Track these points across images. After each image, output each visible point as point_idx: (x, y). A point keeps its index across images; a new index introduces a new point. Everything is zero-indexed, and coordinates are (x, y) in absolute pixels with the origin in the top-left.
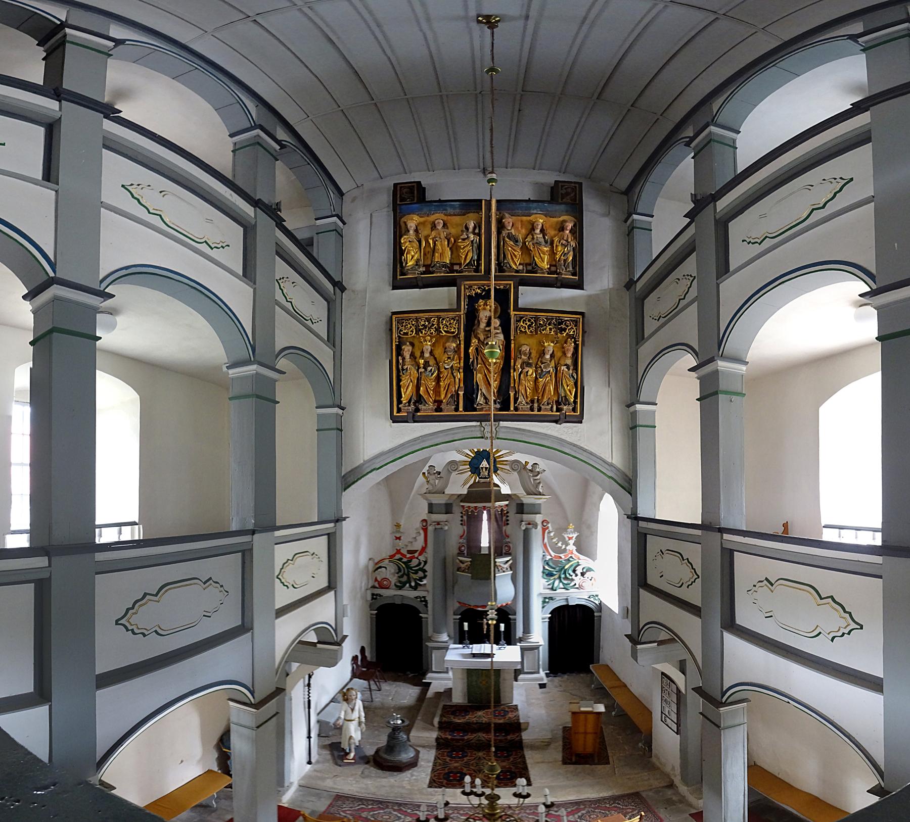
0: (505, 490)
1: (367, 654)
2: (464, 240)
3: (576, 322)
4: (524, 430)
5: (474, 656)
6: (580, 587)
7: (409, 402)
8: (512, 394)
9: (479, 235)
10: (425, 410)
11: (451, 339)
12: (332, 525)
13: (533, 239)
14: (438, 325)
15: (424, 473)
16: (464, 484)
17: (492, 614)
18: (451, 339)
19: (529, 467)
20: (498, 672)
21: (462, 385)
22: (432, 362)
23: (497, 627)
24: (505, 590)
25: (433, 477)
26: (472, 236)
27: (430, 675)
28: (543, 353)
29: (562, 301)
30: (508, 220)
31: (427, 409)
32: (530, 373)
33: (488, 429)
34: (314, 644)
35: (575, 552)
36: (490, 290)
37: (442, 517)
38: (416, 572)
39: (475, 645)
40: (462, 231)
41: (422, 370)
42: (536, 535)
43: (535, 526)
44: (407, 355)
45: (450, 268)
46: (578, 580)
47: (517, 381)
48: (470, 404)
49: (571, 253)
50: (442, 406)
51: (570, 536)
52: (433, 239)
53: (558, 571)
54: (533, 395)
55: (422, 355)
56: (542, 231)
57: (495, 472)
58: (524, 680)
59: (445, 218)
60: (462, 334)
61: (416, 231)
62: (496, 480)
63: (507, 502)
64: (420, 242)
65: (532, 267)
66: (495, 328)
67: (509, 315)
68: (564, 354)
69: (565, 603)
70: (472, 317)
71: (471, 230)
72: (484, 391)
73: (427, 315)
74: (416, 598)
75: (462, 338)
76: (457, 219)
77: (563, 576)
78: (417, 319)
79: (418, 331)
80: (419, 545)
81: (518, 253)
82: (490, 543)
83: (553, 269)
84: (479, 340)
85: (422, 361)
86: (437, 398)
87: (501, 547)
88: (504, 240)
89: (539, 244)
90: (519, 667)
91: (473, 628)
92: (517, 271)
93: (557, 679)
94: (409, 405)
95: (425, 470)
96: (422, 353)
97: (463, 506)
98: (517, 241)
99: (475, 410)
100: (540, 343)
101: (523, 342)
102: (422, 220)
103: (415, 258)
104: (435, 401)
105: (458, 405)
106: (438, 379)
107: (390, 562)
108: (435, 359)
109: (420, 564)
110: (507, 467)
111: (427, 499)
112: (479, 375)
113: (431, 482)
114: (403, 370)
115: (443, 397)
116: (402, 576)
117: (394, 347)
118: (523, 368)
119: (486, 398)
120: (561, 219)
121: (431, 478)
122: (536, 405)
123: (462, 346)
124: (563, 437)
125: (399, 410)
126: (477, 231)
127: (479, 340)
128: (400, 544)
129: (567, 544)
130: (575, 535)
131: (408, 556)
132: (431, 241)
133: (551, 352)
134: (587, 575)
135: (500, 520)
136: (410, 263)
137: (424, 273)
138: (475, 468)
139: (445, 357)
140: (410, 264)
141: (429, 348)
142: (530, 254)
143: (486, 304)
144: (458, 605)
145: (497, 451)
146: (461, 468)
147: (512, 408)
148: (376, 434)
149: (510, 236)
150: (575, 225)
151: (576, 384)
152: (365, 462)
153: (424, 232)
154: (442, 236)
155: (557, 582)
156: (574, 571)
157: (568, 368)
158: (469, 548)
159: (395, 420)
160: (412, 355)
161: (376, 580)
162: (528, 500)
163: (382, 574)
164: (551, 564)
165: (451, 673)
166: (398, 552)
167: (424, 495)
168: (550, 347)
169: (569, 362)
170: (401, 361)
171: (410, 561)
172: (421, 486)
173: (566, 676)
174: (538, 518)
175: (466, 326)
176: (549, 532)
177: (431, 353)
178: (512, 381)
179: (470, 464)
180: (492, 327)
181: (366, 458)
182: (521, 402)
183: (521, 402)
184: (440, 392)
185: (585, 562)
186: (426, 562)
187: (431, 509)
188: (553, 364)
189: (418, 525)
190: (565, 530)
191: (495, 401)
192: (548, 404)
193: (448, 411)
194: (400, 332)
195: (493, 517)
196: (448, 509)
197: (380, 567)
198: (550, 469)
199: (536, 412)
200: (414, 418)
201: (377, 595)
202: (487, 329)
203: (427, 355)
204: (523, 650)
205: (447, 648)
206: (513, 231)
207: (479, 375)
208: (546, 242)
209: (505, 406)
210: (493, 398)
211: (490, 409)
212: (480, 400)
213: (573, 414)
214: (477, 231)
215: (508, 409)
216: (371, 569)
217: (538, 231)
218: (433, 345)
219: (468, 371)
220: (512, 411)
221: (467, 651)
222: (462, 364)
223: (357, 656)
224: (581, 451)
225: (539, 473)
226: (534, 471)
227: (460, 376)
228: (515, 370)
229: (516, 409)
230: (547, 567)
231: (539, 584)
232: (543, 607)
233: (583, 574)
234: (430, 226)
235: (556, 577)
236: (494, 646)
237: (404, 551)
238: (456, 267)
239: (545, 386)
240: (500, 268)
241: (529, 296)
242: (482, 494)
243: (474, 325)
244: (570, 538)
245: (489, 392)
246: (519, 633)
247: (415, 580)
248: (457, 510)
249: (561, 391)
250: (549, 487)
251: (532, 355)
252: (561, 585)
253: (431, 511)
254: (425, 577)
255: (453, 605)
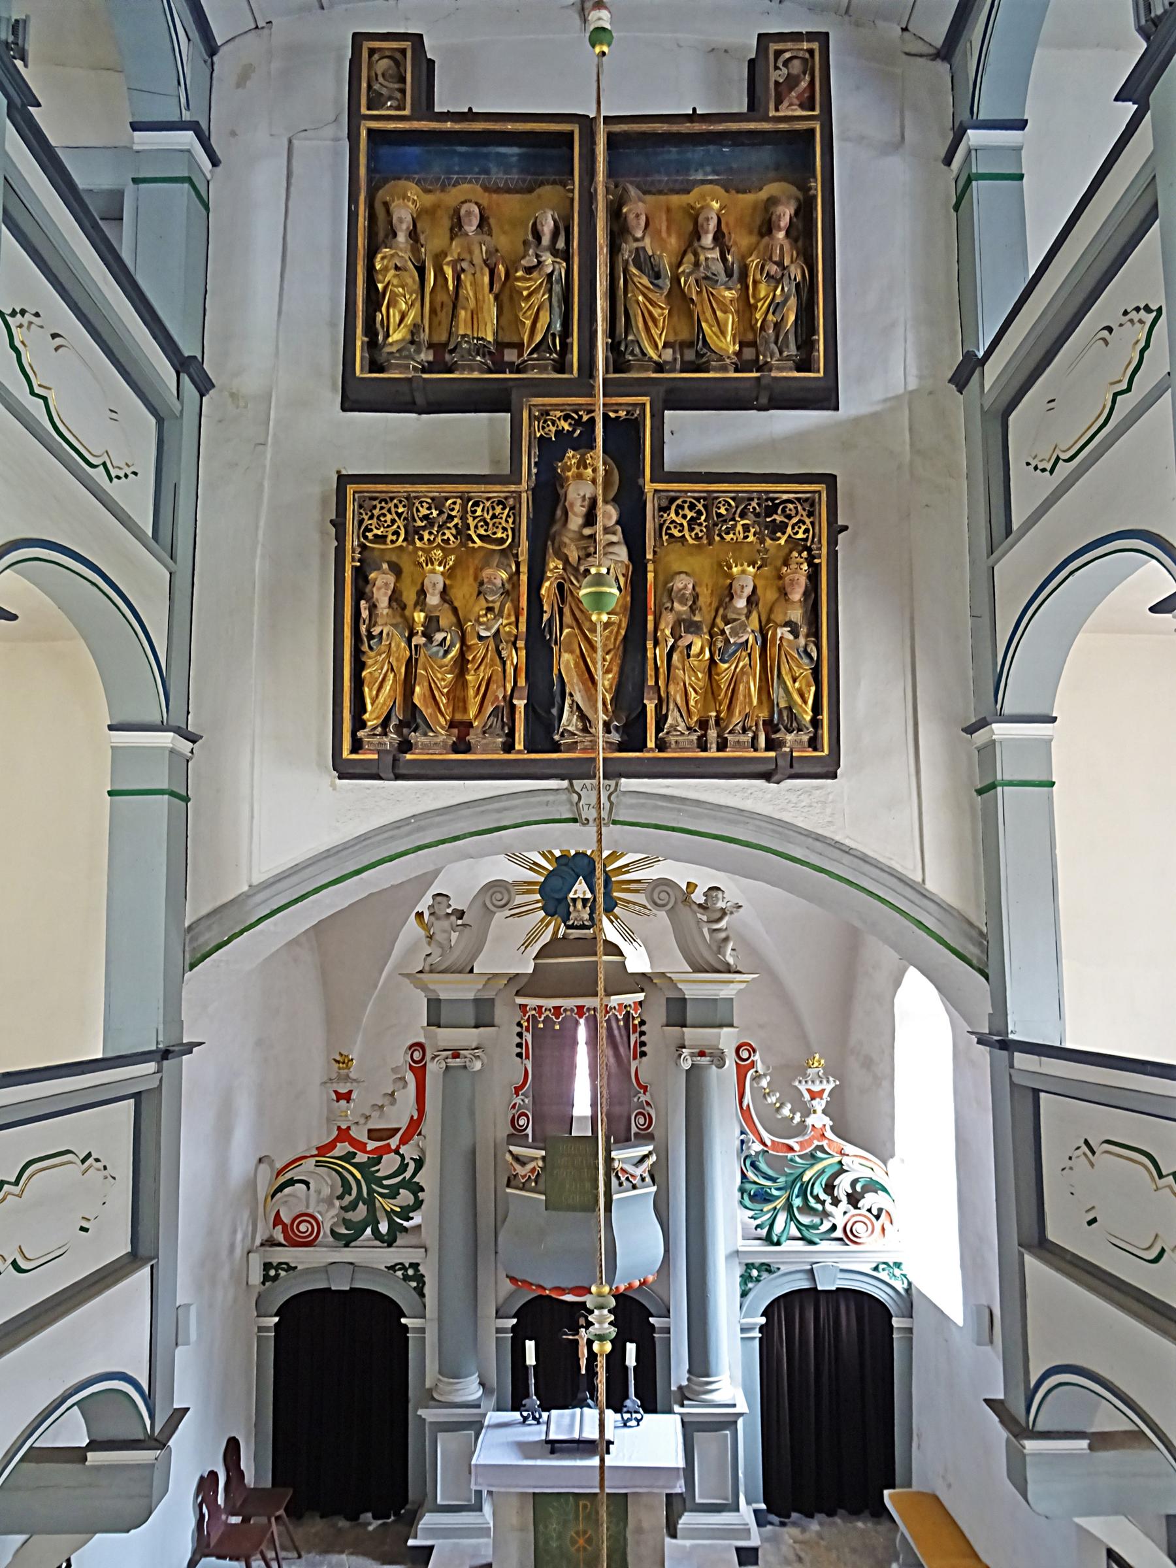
0: (637, 961)
1: (246, 1464)
2: (529, 270)
3: (811, 505)
4: (683, 800)
5: (554, 1447)
6: (849, 1237)
7: (385, 724)
8: (650, 707)
9: (566, 256)
10: (426, 747)
11: (496, 560)
12: (151, 1067)
13: (697, 264)
14: (463, 518)
15: (420, 915)
16: (527, 944)
17: (602, 1323)
18: (496, 560)
19: (698, 897)
20: (620, 1502)
21: (522, 682)
22: (446, 620)
23: (617, 1355)
24: (639, 1242)
25: (445, 924)
26: (548, 259)
27: (429, 1520)
28: (730, 594)
29: (773, 446)
30: (636, 209)
31: (432, 744)
32: (695, 649)
33: (589, 798)
34: (77, 1455)
35: (829, 1134)
36: (592, 421)
37: (468, 1036)
38: (393, 1193)
39: (554, 1413)
40: (525, 243)
41: (419, 640)
42: (721, 1083)
43: (719, 1059)
44: (382, 599)
45: (494, 355)
46: (840, 1215)
47: (663, 670)
48: (543, 734)
49: (793, 301)
50: (472, 738)
51: (816, 1088)
52: (454, 264)
53: (790, 1191)
54: (706, 708)
55: (421, 602)
56: (719, 237)
57: (609, 910)
58: (695, 1533)
59: (485, 199)
60: (524, 545)
61: (413, 235)
62: (611, 933)
63: (640, 996)
64: (421, 271)
65: (696, 354)
66: (607, 530)
67: (642, 492)
68: (784, 593)
69: (806, 1285)
70: (549, 496)
71: (546, 240)
72: (578, 698)
73: (435, 490)
74: (392, 1268)
75: (523, 557)
76: (511, 204)
77: (797, 1202)
78: (409, 500)
79: (413, 533)
80: (400, 1115)
81: (660, 313)
82: (594, 1105)
83: (749, 353)
84: (566, 561)
85: (419, 617)
86: (459, 717)
87: (624, 1121)
88: (626, 271)
89: (711, 279)
90: (679, 1487)
91: (550, 1361)
92: (660, 368)
93: (789, 1534)
94: (385, 734)
95: (423, 906)
96: (422, 592)
97: (523, 1007)
98: (658, 276)
99: (556, 748)
100: (723, 569)
101: (676, 567)
102: (429, 199)
103: (409, 320)
104: (452, 724)
105: (511, 734)
106: (462, 663)
107: (318, 1164)
108: (455, 610)
109: (403, 1167)
110: (641, 898)
111: (424, 988)
112: (566, 656)
113: (439, 937)
114: (370, 636)
115: (472, 712)
116: (353, 1206)
117: (348, 574)
118: (677, 637)
119: (583, 717)
120: (763, 195)
121: (439, 927)
122: (712, 734)
123: (524, 578)
124: (787, 817)
125: (357, 746)
126: (561, 244)
127: (566, 561)
128: (349, 1113)
129: (808, 1112)
130: (828, 1087)
131: (372, 1145)
132: (449, 272)
133: (748, 591)
134: (870, 1200)
135: (623, 1041)
136: (397, 336)
137: (428, 368)
138: (554, 900)
139: (479, 608)
140: (395, 337)
141: (440, 581)
142: (690, 314)
143: (582, 464)
144: (508, 1286)
145: (614, 856)
146: (519, 899)
147: (651, 744)
148: (291, 809)
149: (644, 262)
150: (797, 213)
151: (816, 673)
152: (255, 889)
153: (435, 240)
154: (478, 260)
155: (782, 1218)
156: (829, 1188)
157: (795, 633)
158: (538, 1119)
159: (345, 771)
160: (395, 598)
161: (278, 1220)
162: (696, 988)
163: (292, 1203)
164: (763, 1166)
165: (487, 1508)
166: (344, 1135)
167: (416, 978)
168: (746, 576)
169: (796, 614)
170: (365, 614)
171: (378, 1161)
172: (412, 950)
173: (814, 1526)
174: (727, 1039)
175: (533, 524)
176: (757, 1077)
177: (444, 593)
178: (650, 672)
179: (543, 889)
180: (599, 527)
181: (257, 879)
182: (674, 728)
183: (674, 728)
184: (465, 701)
185: (859, 1164)
186: (419, 1163)
187: (436, 1015)
188: (754, 623)
189: (401, 1058)
190: (802, 1071)
191: (607, 725)
192: (744, 730)
193: (487, 750)
194: (366, 525)
195: (602, 1032)
196: (482, 1014)
197: (291, 1182)
198: (752, 902)
199: (713, 753)
200: (397, 768)
201: (279, 1266)
202: (587, 531)
203: (433, 600)
204: (689, 1428)
205: (477, 1426)
206: (647, 243)
207: (566, 656)
208: (729, 274)
209: (632, 738)
210: (602, 717)
211: (593, 747)
212: (569, 721)
213: (810, 753)
214: (561, 244)
215: (642, 747)
216: (262, 1191)
217: (708, 240)
218: (450, 574)
219: (539, 644)
220: (651, 752)
221: (535, 1433)
222: (523, 628)
223: (213, 1475)
224: (837, 854)
225: (724, 912)
226: (711, 908)
227: (517, 657)
228: (656, 643)
229: (661, 746)
230: (751, 1175)
231: (731, 1226)
232: (744, 1294)
233: (854, 1200)
234: (446, 223)
235: (779, 1203)
236: (609, 1413)
237: (360, 1134)
238: (510, 356)
239: (735, 681)
240: (618, 362)
241: (694, 438)
242: (573, 966)
243: (552, 520)
244: (814, 1095)
245: (592, 700)
246: (680, 1375)
247: (389, 1214)
248: (505, 1015)
249: (778, 695)
250: (749, 948)
251: (702, 601)
252: (794, 1231)
253: (434, 1021)
254: (418, 1204)
255: (497, 1289)
